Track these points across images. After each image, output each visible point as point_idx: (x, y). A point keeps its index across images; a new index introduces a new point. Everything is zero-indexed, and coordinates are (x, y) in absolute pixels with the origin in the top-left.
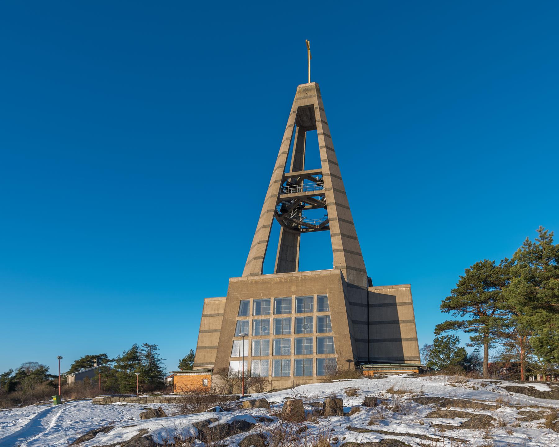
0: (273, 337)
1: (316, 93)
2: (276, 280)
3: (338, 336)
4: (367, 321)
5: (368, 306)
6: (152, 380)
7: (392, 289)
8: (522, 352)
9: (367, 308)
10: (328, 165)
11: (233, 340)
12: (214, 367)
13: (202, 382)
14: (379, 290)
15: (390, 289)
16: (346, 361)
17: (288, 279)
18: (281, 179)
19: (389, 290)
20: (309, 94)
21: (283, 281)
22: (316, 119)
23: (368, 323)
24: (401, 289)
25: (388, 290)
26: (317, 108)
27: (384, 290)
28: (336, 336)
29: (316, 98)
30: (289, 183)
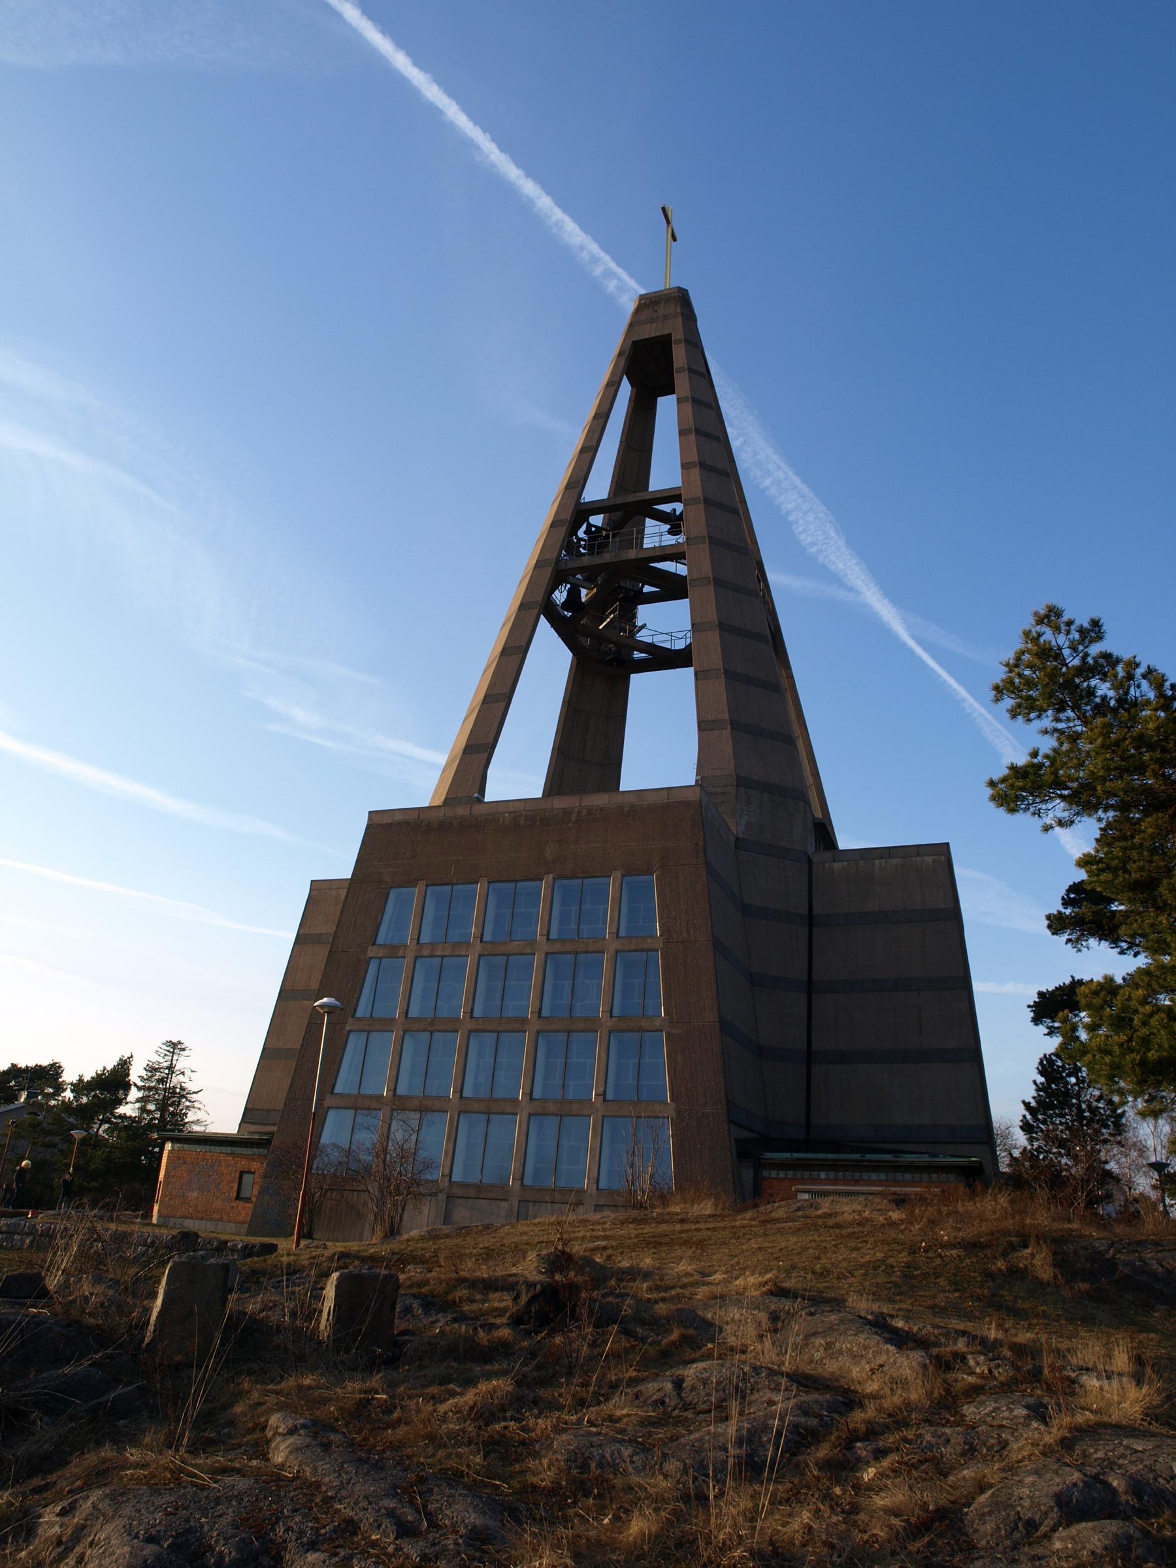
0: (469, 1027)
1: (679, 310)
2: (501, 822)
3: (679, 1031)
4: (806, 978)
5: (811, 920)
6: (1075, 1064)
7: (890, 860)
8: (782, 1374)
9: (807, 929)
10: (698, 477)
11: (348, 1028)
12: (274, 1129)
13: (237, 1181)
14: (845, 864)
15: (883, 860)
16: (1024, 1102)
17: (538, 818)
18: (569, 517)
19: (880, 863)
20: (661, 310)
21: (522, 823)
22: (675, 365)
23: (810, 987)
24: (919, 859)
25: (877, 862)
26: (678, 342)
27: (862, 862)
28: (674, 1031)
29: (680, 319)
30: (593, 529)
